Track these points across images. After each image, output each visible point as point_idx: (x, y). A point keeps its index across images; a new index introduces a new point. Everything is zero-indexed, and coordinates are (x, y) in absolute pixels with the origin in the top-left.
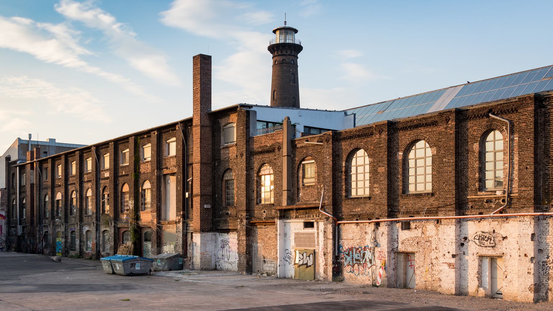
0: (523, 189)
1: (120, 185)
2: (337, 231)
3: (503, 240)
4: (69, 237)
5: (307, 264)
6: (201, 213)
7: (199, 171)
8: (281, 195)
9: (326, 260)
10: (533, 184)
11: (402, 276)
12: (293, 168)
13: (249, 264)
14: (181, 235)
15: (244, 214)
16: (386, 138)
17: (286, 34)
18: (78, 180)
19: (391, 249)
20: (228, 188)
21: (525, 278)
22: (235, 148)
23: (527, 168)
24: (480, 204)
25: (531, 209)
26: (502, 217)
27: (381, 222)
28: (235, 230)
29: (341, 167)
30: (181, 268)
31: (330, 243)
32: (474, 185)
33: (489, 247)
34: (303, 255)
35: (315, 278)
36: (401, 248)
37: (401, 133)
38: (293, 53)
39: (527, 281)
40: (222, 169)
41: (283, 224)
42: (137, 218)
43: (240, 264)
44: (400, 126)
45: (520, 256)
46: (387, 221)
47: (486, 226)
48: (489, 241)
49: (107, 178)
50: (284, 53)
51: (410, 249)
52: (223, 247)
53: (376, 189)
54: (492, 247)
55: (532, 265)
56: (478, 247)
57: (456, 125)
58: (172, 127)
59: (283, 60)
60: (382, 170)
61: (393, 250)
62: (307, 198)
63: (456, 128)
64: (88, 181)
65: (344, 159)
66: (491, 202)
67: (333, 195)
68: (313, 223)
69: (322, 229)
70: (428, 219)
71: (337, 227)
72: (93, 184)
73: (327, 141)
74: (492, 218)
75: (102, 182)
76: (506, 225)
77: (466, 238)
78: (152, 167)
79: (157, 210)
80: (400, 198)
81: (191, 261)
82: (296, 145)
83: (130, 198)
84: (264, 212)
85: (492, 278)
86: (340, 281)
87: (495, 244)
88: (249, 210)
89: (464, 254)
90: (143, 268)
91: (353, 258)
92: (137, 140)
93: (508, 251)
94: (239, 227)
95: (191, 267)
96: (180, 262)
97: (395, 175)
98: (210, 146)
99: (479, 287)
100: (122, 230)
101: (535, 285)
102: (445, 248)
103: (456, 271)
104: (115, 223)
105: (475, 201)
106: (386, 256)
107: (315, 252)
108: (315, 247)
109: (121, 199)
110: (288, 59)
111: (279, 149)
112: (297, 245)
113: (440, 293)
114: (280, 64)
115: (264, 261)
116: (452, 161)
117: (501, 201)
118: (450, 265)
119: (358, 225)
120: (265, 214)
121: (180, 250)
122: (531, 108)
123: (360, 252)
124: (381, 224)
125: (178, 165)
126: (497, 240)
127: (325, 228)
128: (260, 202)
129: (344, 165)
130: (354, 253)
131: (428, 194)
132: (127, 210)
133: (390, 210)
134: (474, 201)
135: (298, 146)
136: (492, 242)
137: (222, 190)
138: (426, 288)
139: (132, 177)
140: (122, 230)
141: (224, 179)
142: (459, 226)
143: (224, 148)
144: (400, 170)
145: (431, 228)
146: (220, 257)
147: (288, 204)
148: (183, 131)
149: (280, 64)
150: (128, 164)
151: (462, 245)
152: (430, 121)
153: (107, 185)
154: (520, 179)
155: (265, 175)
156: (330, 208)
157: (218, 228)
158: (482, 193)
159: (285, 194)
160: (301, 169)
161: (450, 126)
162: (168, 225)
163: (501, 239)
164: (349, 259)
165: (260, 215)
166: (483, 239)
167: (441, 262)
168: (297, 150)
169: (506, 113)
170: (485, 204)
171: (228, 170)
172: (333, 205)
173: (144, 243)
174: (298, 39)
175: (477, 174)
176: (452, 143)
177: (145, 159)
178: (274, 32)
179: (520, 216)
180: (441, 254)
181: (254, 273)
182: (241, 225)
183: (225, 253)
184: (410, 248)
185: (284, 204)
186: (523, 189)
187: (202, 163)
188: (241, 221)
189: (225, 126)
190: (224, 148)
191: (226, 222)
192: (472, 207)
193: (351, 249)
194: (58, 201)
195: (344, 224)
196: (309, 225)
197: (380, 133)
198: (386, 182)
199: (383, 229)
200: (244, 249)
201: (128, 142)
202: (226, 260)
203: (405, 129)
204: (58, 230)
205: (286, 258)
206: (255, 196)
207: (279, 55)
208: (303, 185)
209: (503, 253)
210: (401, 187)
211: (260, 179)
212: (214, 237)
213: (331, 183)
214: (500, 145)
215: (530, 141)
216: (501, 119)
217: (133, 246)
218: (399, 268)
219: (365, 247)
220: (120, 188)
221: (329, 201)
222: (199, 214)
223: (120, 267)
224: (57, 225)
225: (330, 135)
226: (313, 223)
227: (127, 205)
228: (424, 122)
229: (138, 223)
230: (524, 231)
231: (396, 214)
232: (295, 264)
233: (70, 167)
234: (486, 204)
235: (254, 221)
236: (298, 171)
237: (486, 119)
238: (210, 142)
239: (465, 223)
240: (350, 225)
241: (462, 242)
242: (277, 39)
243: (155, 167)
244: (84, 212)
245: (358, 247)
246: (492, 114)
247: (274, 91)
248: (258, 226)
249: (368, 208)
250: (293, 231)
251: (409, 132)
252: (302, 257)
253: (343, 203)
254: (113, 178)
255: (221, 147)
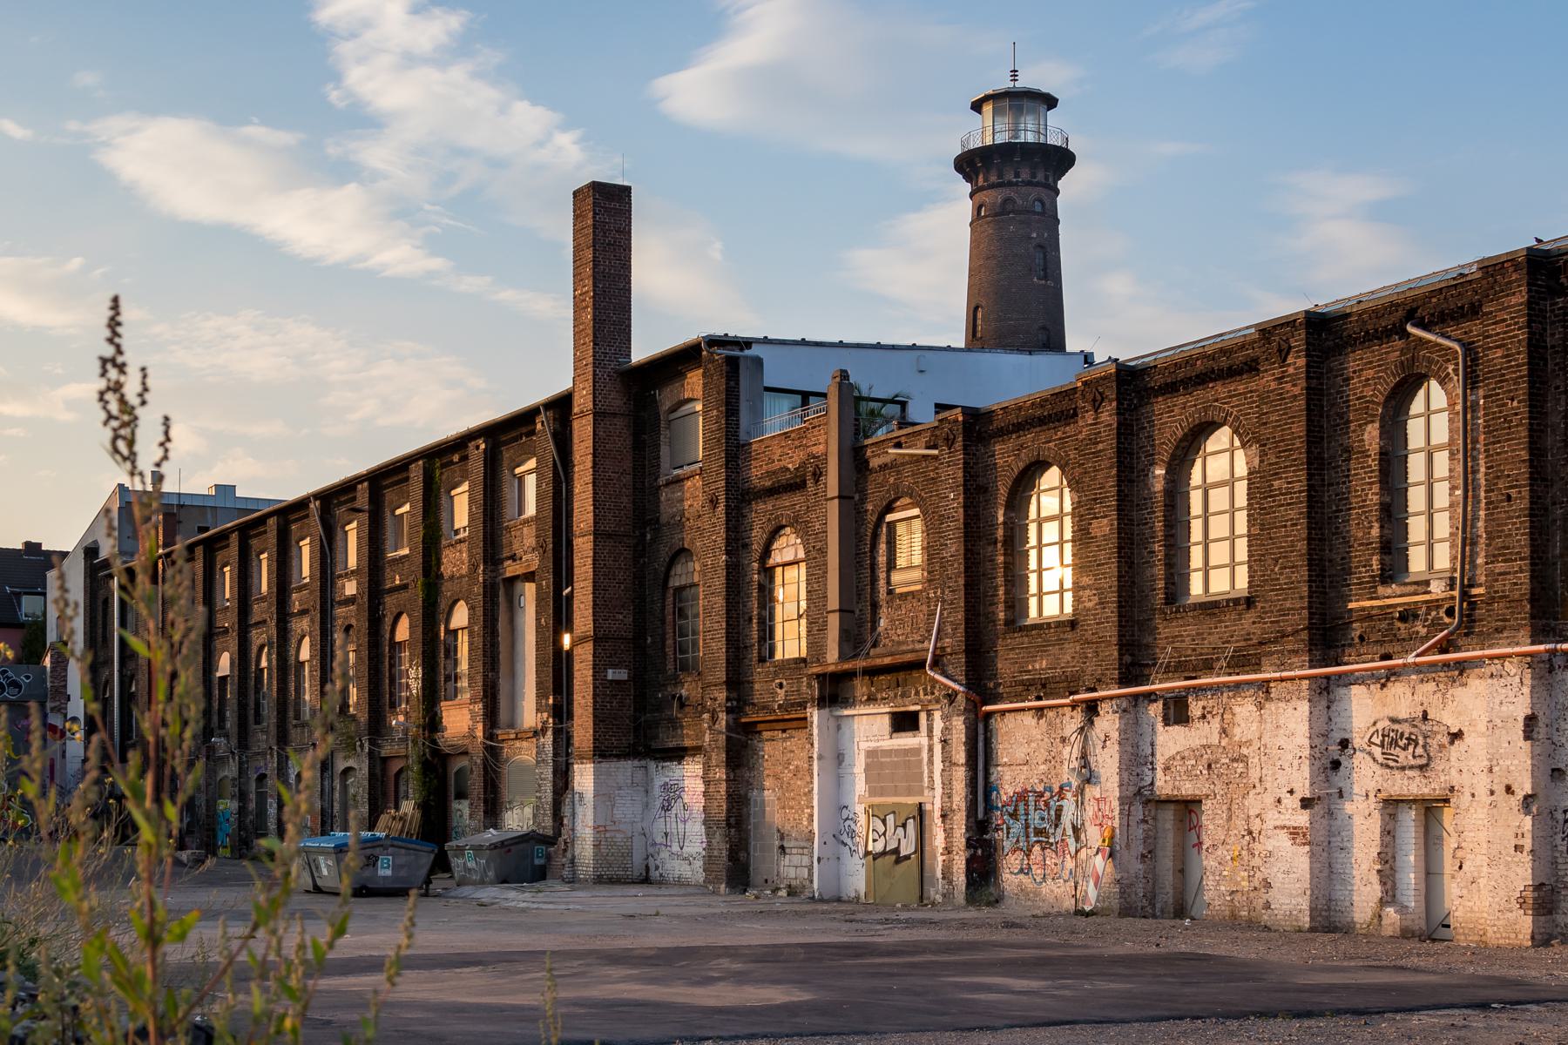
0: (1500, 567)
1: (388, 620)
2: (981, 738)
3: (1452, 743)
4: (253, 796)
5: (896, 851)
6: (595, 696)
7: (590, 561)
8: (823, 629)
9: (949, 834)
10: (1526, 551)
11: (1168, 879)
12: (860, 539)
13: (738, 855)
14: (548, 772)
15: (722, 696)
16: (1113, 420)
17: (1018, 111)
18: (274, 609)
19: (1132, 789)
20: (682, 613)
21: (1507, 864)
22: (697, 481)
23: (1509, 498)
24: (1384, 625)
25: (1524, 635)
26: (1446, 665)
27: (1103, 699)
28: (697, 750)
29: (994, 525)
30: (539, 875)
31: (960, 774)
32: (1368, 564)
33: (1412, 767)
34: (884, 822)
35: (921, 898)
36: (1164, 785)
37: (1159, 405)
38: (1040, 177)
39: (1512, 875)
40: (664, 553)
41: (832, 723)
42: (433, 723)
43: (709, 861)
44: (1157, 380)
45: (1492, 793)
46: (1119, 697)
47: (1402, 700)
48: (1411, 748)
49: (351, 600)
50: (1010, 176)
51: (1188, 789)
52: (666, 808)
53: (1088, 592)
54: (1421, 768)
55: (1528, 820)
56: (1376, 767)
57: (1308, 365)
58: (522, 422)
59: (1006, 201)
60: (1104, 527)
61: (1139, 793)
62: (898, 634)
63: (1308, 378)
64: (303, 612)
65: (1002, 500)
66: (1416, 616)
67: (967, 620)
68: (915, 715)
69: (940, 735)
70: (1238, 685)
71: (981, 727)
72: (312, 621)
73: (950, 442)
74: (1418, 669)
75: (340, 611)
76: (1458, 692)
77: (1344, 744)
78: (471, 556)
79: (485, 696)
80: (1158, 620)
81: (569, 855)
82: (867, 462)
83: (411, 661)
84: (781, 686)
85: (1428, 874)
86: (989, 904)
87: (1429, 758)
88: (737, 682)
89: (1341, 795)
90: (403, 873)
91: (1027, 827)
92: (433, 471)
93: (1466, 779)
94: (707, 738)
95: (566, 873)
96: (532, 860)
97: (1145, 542)
98: (627, 479)
99: (1382, 903)
100: (395, 767)
101: (1538, 887)
102: (1282, 780)
103: (1312, 854)
104: (372, 742)
105: (1370, 617)
106: (1117, 812)
107: (921, 813)
108: (922, 794)
109: (392, 666)
110: (1027, 197)
111: (818, 475)
112: (873, 792)
113: (1267, 928)
114: (996, 215)
115: (782, 848)
116: (1297, 486)
117: (1442, 613)
118: (1294, 833)
119: (1041, 717)
120: (782, 693)
121: (548, 822)
122: (1519, 298)
123: (1047, 804)
124: (1104, 708)
125: (541, 546)
126: (1434, 743)
127: (946, 730)
128: (772, 654)
129: (1001, 519)
130: (1031, 808)
131: (1236, 601)
132: (408, 700)
133: (1127, 659)
134: (1367, 616)
135: (875, 463)
136: (1419, 751)
137: (663, 622)
138: (1234, 916)
139: (417, 594)
140: (395, 767)
141: (671, 584)
142: (1324, 703)
143: (668, 484)
144: (1159, 525)
145: (1244, 709)
146: (659, 840)
147: (842, 657)
148: (555, 435)
149: (996, 215)
150: (406, 551)
151: (1336, 765)
152: (1240, 357)
153: (354, 622)
154: (1490, 538)
155: (784, 565)
156: (957, 665)
157: (654, 745)
158: (1389, 591)
159: (834, 621)
160: (883, 538)
161: (1291, 370)
162: (518, 744)
163: (1445, 740)
164: (1017, 827)
165: (767, 698)
166: (1394, 743)
167: (1270, 824)
168: (871, 478)
169: (1453, 319)
170: (1398, 624)
171: (682, 553)
172: (967, 652)
173: (455, 805)
174: (1056, 128)
175: (1376, 525)
176: (1299, 428)
177: (457, 532)
178: (977, 106)
179: (1491, 658)
180: (1269, 799)
181: (755, 887)
182: (710, 731)
183: (671, 827)
184: (1188, 785)
185: (832, 655)
186: (1500, 567)
187: (598, 534)
188: (714, 719)
189: (674, 409)
190: (668, 484)
191: (675, 724)
192: (1361, 638)
193: (1022, 796)
194: (223, 679)
195: (1003, 712)
196: (904, 722)
197: (1096, 406)
198: (1112, 569)
199: (1108, 723)
200: (721, 807)
201: (407, 479)
202: (675, 848)
203: (1170, 389)
204: (221, 774)
205: (840, 835)
206: (755, 635)
207: (992, 186)
208: (890, 592)
209: (1452, 789)
210: (1161, 584)
211: (772, 579)
212: (640, 774)
213: (961, 581)
214: (1441, 430)
215: (1518, 406)
216: (1441, 340)
217: (418, 815)
218: (1160, 853)
219: (1061, 788)
220: (388, 628)
221: (954, 641)
222: (590, 700)
223: (328, 866)
224: (221, 758)
225: (956, 421)
226: (915, 715)
227: (408, 686)
228: (1224, 362)
229: (434, 742)
230: (1504, 708)
231: (1146, 672)
232: (867, 853)
233: (255, 569)
234: (1402, 626)
235: (751, 717)
236: (874, 546)
237: (1399, 344)
238: (628, 465)
239: (1342, 691)
240: (1020, 716)
241: (1332, 758)
242: (985, 131)
243: (480, 557)
244: (291, 714)
245: (1040, 788)
246: (1414, 325)
247: (976, 309)
248: (766, 735)
249: (1067, 656)
250: (864, 746)
251: (1182, 400)
252: (881, 829)
253: (1000, 646)
254: (366, 599)
255: (662, 481)
